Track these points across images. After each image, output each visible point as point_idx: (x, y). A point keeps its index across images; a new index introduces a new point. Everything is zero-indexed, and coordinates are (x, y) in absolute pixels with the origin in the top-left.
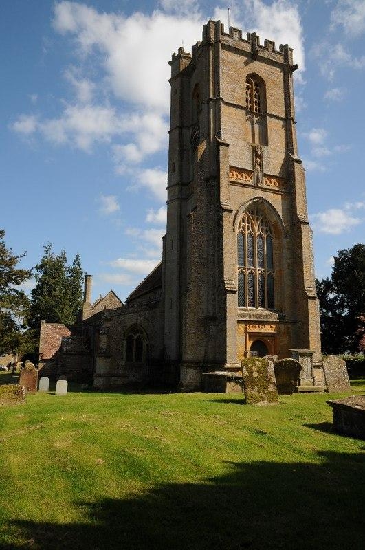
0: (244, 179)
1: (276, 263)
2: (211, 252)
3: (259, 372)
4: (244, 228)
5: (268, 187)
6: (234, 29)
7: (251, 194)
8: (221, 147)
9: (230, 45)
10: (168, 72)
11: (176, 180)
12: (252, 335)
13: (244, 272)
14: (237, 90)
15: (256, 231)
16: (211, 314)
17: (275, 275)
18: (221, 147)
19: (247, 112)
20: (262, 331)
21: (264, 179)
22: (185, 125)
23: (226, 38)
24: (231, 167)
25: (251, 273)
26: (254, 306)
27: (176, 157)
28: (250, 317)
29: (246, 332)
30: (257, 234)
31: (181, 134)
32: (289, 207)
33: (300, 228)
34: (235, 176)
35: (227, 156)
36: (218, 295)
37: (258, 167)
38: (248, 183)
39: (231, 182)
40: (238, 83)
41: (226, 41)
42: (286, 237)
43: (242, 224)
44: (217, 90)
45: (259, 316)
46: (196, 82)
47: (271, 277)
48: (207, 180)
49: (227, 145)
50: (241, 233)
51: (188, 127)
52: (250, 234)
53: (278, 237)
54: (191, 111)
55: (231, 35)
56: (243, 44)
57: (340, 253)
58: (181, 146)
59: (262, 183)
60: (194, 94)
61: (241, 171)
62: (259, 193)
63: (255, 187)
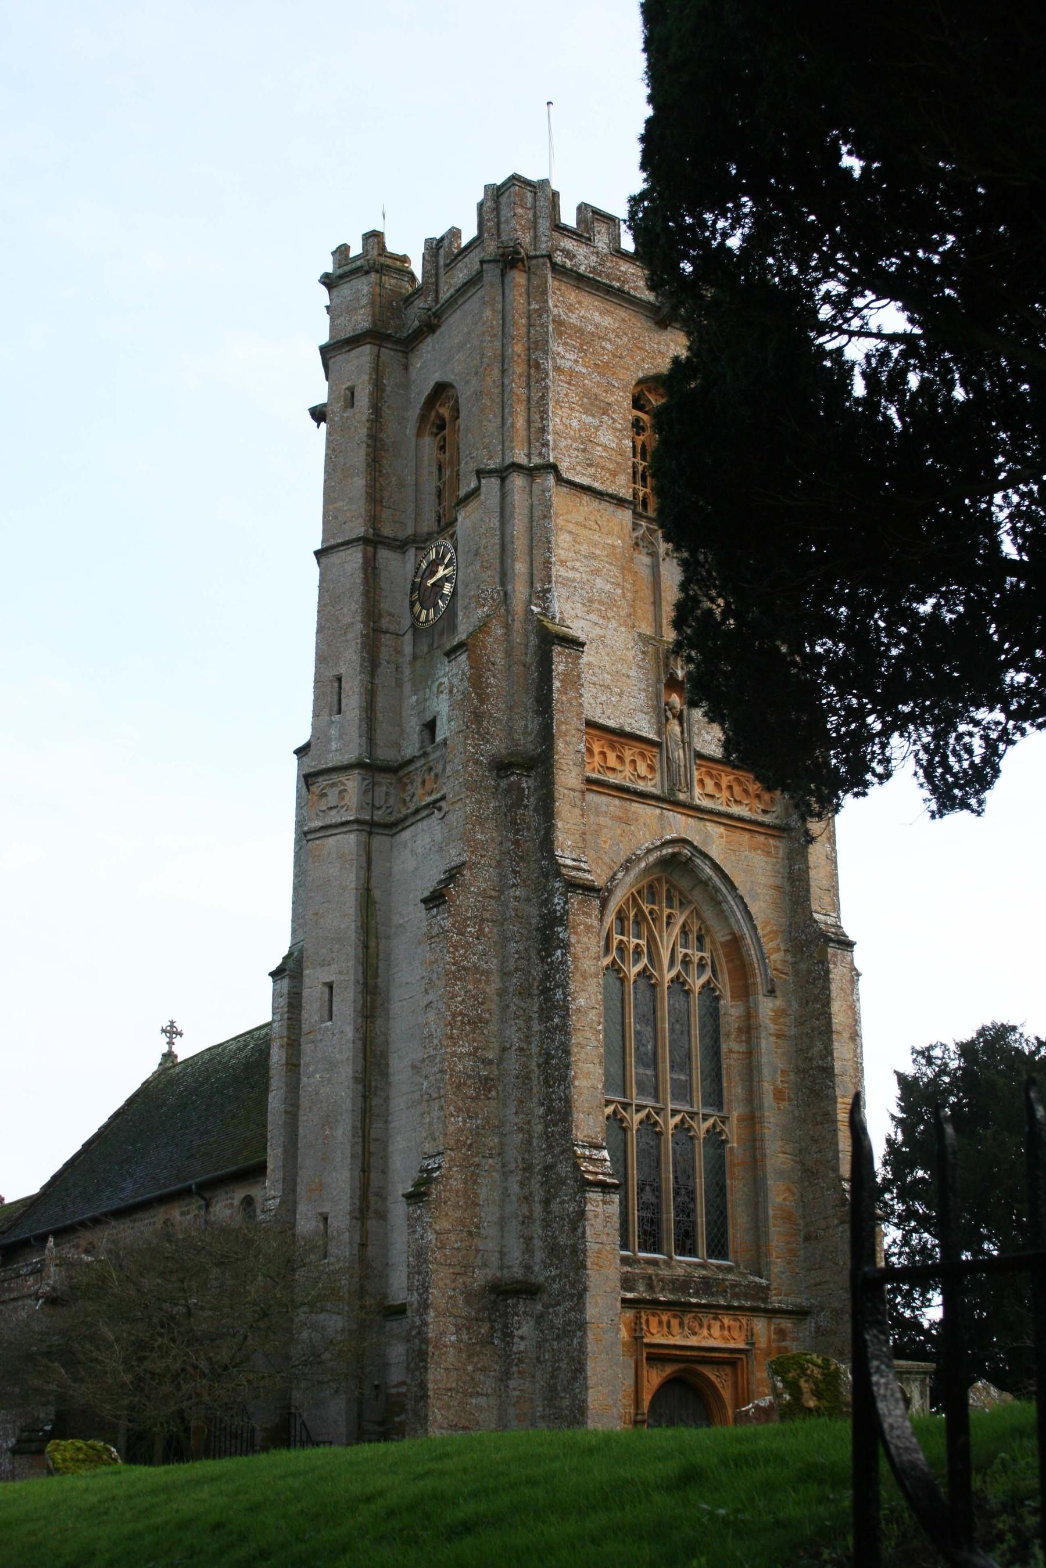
0: (636, 771)
1: (734, 1089)
2: (514, 1037)
3: (817, 1394)
4: (686, 962)
5: (706, 803)
6: (596, 212)
7: (652, 828)
8: (557, 649)
9: (582, 269)
10: (310, 320)
11: (346, 747)
12: (658, 1356)
13: (656, 1124)
14: (606, 437)
15: (666, 962)
16: (518, 1272)
17: (733, 1133)
18: (557, 649)
19: (636, 515)
20: (693, 1341)
21: (696, 775)
22: (387, 531)
23: (568, 244)
24: (590, 724)
25: (648, 1123)
26: (657, 1248)
27: (350, 661)
28: (650, 1287)
29: (637, 1340)
30: (668, 976)
31: (371, 570)
32: (778, 882)
33: (823, 961)
34: (597, 758)
35: (574, 681)
36: (547, 1202)
37: (675, 727)
38: (641, 786)
39: (589, 781)
40: (606, 410)
41: (569, 254)
42: (772, 992)
43: (617, 937)
44: (538, 433)
45: (682, 1285)
46: (437, 377)
47: (716, 1140)
48: (502, 767)
49: (575, 644)
50: (614, 968)
51: (400, 546)
52: (643, 974)
53: (744, 991)
54: (410, 479)
55: (582, 234)
56: (625, 267)
57: (925, 1054)
58: (372, 614)
59: (690, 789)
60: (423, 418)
61: (619, 737)
62: (681, 825)
63: (668, 801)
